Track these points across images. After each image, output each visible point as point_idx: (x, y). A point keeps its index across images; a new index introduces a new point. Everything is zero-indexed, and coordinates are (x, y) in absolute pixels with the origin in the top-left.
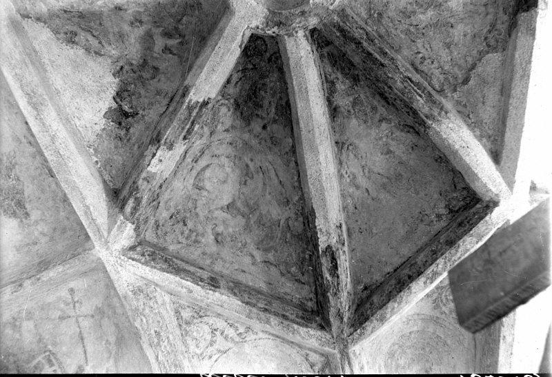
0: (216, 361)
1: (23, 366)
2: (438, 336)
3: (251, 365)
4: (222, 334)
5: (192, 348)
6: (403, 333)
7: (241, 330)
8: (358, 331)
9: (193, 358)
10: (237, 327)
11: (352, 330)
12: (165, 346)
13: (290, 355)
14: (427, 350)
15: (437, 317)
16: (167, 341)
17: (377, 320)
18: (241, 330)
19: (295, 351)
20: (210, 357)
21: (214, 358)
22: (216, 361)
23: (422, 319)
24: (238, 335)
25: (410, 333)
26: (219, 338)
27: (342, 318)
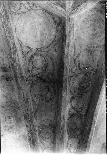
0: (21, 16)
1: (47, 42)
2: (101, 18)
3: (97, 69)
4: (24, 6)
5: (12, 10)
6: (89, 15)
7: (31, 5)
8: (75, 10)
9: (12, 14)
10: (30, 4)
11: (73, 9)
12: (2, 7)
13: (48, 17)
14: (96, 22)
15: (102, 11)
16: (3, 5)
17: (83, 6)
18: (31, 5)
19: (50, 16)
20: (19, 14)
21: (20, 15)
22: (21, 16)
23: (97, 11)
24: (30, 7)
25: (92, 15)
26: (23, 7)
27: (70, 4)
